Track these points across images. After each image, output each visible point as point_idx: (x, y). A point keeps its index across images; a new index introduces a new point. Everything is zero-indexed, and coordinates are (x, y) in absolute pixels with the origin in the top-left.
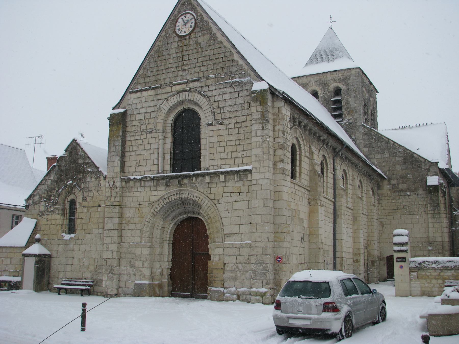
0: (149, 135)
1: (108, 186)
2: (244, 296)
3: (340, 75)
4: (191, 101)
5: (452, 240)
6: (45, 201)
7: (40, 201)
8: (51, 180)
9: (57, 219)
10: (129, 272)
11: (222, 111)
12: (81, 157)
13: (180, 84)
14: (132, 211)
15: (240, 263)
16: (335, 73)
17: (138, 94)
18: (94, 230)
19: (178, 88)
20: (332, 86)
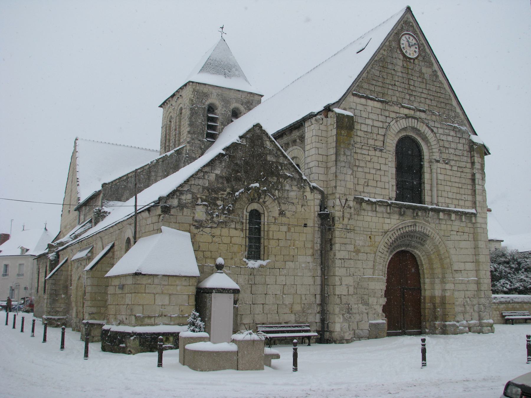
0: (378, 153)
3: (243, 97)
4: (414, 129)
5: (181, 276)
6: (205, 205)
7: (194, 204)
8: (216, 175)
9: (237, 236)
12: (270, 152)
13: (409, 109)
14: (362, 238)
15: (468, 297)
16: (238, 93)
17: (363, 101)
19: (406, 111)
20: (234, 105)
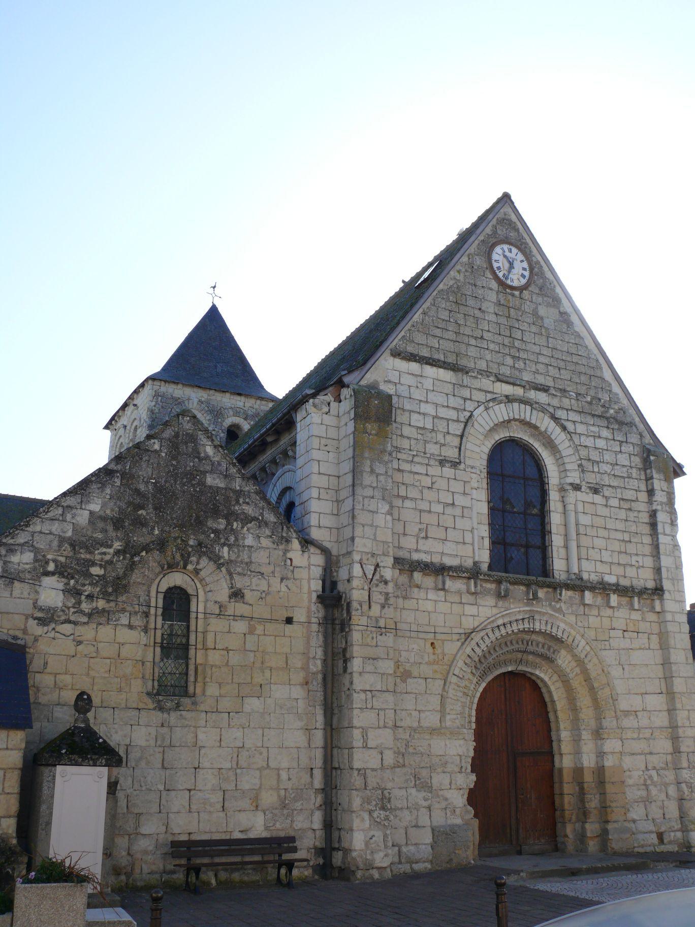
0: (448, 471)
1: (361, 574)
2: (672, 834)
10: (417, 804)
11: (596, 470)
14: (415, 646)
15: (654, 768)
18: (273, 687)
